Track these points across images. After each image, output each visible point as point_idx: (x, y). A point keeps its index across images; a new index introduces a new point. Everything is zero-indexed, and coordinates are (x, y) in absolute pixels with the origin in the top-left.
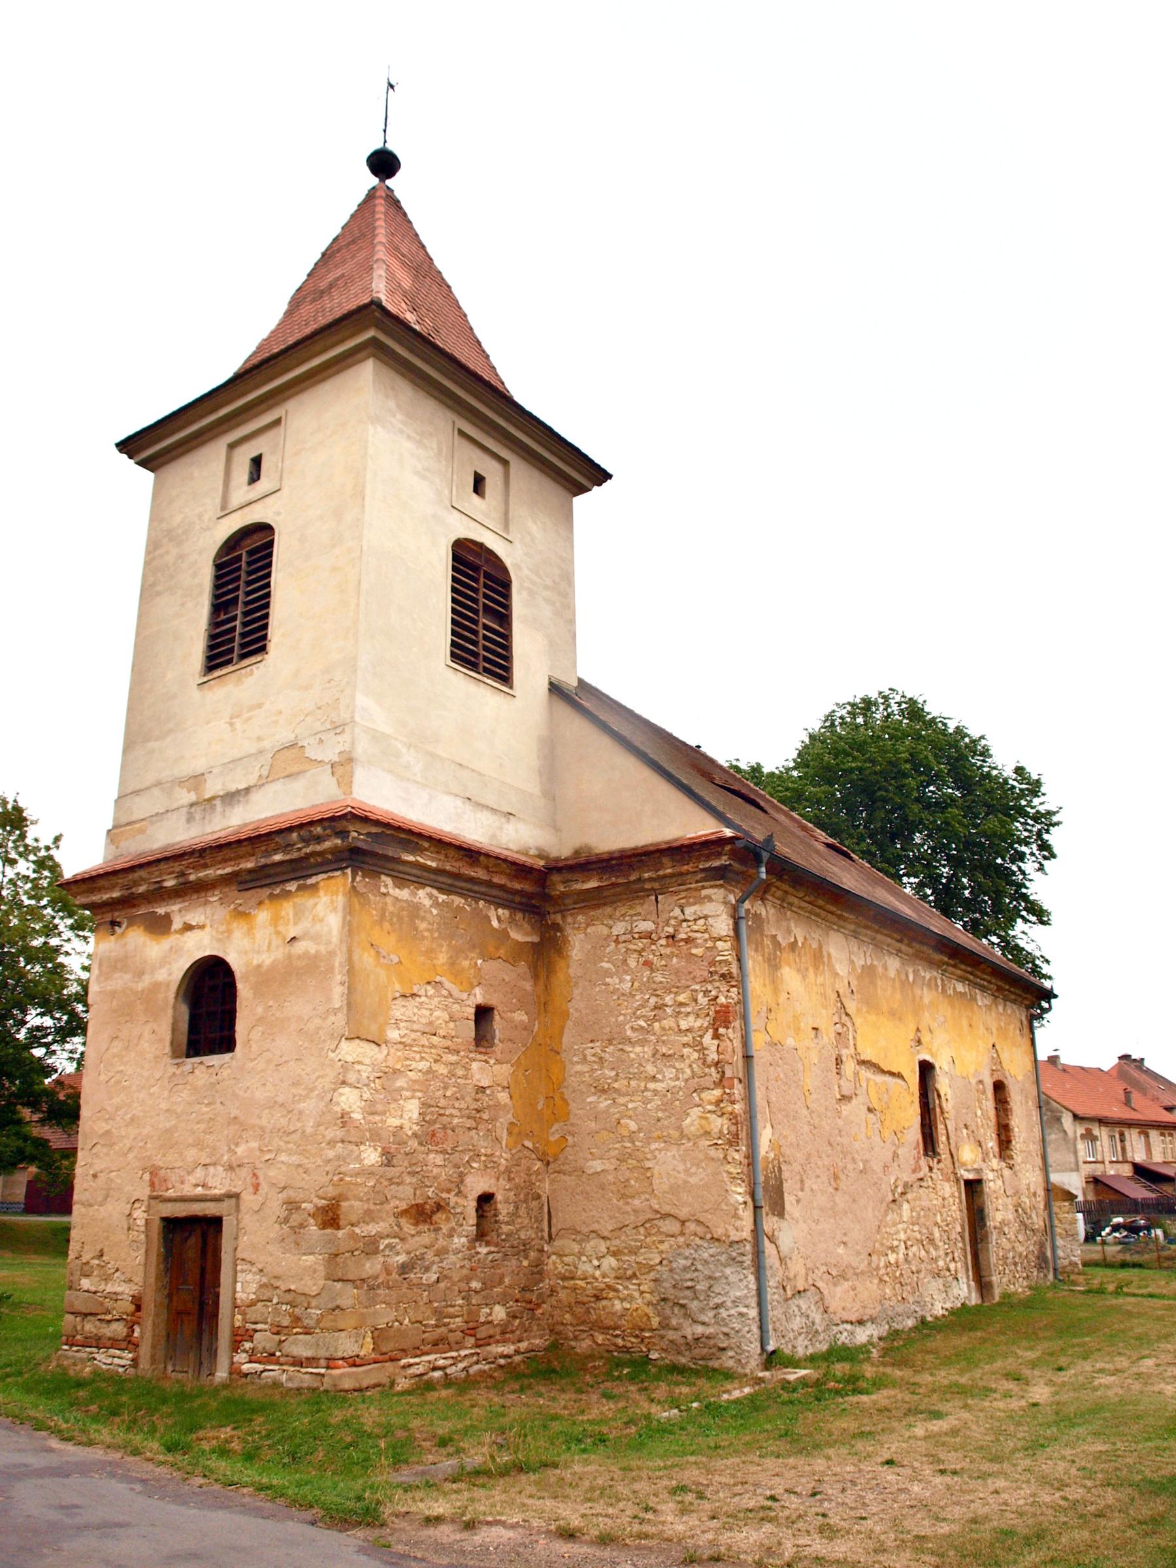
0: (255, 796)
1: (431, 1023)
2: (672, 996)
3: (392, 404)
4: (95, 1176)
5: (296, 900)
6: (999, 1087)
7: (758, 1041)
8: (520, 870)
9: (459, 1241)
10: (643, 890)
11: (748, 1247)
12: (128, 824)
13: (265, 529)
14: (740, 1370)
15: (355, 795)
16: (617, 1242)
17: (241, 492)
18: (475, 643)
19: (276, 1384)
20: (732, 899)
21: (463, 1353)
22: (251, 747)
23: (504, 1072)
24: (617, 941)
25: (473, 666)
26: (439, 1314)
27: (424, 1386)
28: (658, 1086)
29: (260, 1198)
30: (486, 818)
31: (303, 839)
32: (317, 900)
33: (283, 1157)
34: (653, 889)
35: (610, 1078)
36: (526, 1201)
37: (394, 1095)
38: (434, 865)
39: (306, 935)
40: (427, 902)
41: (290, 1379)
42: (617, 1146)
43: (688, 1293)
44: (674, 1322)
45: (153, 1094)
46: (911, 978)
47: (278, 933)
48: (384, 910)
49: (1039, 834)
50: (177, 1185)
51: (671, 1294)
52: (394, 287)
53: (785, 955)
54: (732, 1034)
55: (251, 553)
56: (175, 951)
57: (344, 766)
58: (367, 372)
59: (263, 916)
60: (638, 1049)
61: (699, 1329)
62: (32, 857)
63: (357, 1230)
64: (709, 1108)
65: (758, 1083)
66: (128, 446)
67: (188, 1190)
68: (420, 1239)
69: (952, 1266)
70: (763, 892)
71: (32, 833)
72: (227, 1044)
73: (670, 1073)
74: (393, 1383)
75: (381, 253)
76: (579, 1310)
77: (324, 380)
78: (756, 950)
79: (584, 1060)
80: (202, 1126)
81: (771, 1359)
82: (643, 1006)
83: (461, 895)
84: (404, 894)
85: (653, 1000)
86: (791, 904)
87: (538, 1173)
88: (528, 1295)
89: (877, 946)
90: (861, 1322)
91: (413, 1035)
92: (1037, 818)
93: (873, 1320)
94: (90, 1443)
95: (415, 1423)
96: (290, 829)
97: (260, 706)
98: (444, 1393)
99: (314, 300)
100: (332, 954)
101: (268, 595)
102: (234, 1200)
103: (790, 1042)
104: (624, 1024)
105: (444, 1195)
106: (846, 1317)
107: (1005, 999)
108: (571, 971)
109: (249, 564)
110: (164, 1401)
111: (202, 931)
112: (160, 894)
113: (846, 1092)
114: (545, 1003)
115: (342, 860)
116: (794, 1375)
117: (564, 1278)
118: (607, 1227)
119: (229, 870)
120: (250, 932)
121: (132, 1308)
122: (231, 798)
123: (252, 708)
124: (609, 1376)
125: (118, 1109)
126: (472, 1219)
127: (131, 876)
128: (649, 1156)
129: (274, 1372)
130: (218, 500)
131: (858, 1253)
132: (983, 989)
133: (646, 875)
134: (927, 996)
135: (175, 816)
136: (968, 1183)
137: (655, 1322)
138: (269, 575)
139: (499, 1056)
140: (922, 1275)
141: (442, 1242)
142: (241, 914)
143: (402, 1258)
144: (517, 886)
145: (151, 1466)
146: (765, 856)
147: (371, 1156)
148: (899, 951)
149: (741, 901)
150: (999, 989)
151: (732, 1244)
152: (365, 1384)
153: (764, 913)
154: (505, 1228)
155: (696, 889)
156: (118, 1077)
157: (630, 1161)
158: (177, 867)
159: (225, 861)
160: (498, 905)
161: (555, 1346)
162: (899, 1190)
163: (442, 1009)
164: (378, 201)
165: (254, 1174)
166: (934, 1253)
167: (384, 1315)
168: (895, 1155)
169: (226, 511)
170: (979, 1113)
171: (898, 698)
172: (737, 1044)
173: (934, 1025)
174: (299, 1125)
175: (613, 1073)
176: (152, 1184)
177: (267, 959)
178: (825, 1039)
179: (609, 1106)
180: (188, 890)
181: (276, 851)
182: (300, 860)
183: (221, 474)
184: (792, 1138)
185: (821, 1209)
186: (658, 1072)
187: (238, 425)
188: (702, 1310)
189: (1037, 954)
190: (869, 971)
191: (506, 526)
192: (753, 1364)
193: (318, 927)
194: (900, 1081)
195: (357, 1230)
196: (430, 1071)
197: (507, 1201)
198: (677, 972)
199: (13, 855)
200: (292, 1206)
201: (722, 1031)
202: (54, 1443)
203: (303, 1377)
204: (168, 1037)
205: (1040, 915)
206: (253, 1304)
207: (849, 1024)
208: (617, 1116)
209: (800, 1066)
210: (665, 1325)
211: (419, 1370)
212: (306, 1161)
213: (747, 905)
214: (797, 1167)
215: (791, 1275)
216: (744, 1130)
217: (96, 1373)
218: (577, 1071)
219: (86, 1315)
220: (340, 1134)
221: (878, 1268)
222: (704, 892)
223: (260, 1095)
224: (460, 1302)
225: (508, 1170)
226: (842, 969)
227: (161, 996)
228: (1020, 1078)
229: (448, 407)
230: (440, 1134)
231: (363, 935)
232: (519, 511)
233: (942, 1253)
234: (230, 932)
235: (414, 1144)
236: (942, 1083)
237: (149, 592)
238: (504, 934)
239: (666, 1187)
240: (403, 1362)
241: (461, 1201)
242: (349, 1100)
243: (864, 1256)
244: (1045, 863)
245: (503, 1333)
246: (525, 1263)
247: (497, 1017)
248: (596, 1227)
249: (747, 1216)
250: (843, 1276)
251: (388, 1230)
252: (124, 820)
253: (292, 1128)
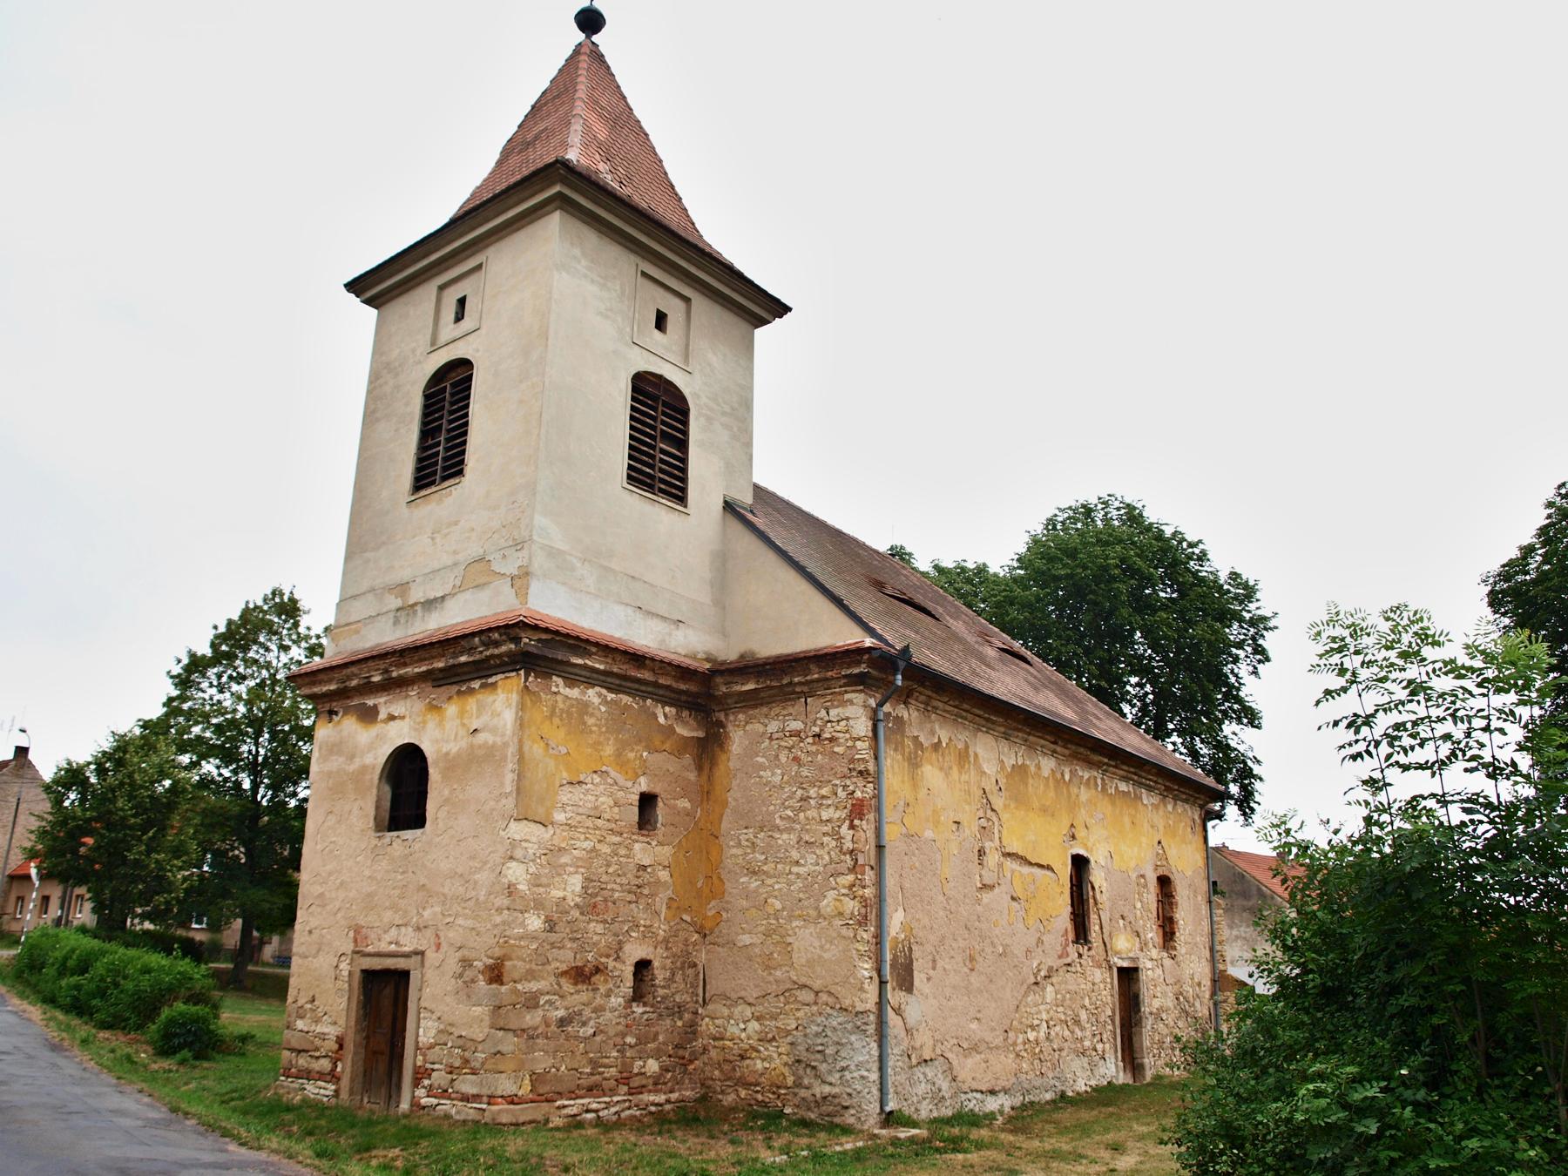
1: (596, 808)
3: (577, 252)
5: (480, 696)
6: (1164, 882)
7: (891, 833)
8: (683, 672)
9: (616, 1001)
10: (794, 693)
11: (872, 1018)
13: (464, 365)
14: (859, 1126)
15: (530, 605)
16: (760, 1008)
17: (448, 330)
18: (652, 467)
19: (447, 1116)
20: (872, 703)
21: (615, 1099)
22: (447, 560)
23: (666, 852)
24: (771, 738)
25: (650, 488)
26: (594, 1064)
27: (575, 1123)
29: (440, 956)
30: (657, 626)
31: (483, 643)
33: (460, 921)
36: (682, 968)
37: (558, 870)
38: (602, 667)
40: (596, 700)
41: (458, 1112)
43: (818, 1056)
44: (806, 1082)
46: (1067, 777)
47: (463, 725)
48: (554, 707)
49: (1254, 639)
51: (804, 1056)
52: (590, 140)
53: (927, 754)
54: (867, 826)
55: (453, 385)
56: (380, 738)
57: (521, 579)
58: (555, 221)
59: (452, 709)
60: (785, 836)
61: (827, 1089)
62: (304, 644)
63: (519, 987)
64: (844, 891)
65: (890, 869)
66: (356, 286)
67: (384, 947)
68: (578, 997)
69: (1099, 1047)
70: (905, 696)
71: (304, 621)
72: (418, 821)
73: (811, 859)
74: (547, 1121)
75: (580, 107)
76: (726, 1067)
77: (518, 229)
78: (896, 750)
79: (739, 845)
80: (397, 892)
81: (889, 1119)
82: (790, 798)
83: (628, 694)
84: (574, 693)
85: (800, 792)
86: (935, 708)
87: (695, 944)
88: (681, 1052)
89: (1031, 747)
90: (992, 1092)
91: (578, 818)
92: (1253, 622)
93: (1006, 1091)
94: (260, 1148)
95: (549, 1153)
96: (473, 634)
97: (456, 523)
98: (590, 1132)
99: (520, 152)
100: (506, 745)
101: (466, 424)
103: (929, 834)
105: (603, 960)
106: (975, 1086)
107: (1175, 799)
108: (731, 764)
109: (452, 395)
110: (353, 1126)
111: (404, 721)
112: (369, 688)
113: (987, 881)
114: (706, 793)
115: (516, 663)
116: (904, 1133)
117: (715, 1039)
118: (752, 994)
119: (424, 668)
120: (441, 724)
121: (336, 1047)
122: (430, 604)
123: (449, 525)
124: (744, 1127)
125: (330, 874)
126: (629, 981)
129: (446, 1106)
130: (429, 337)
131: (993, 1029)
132: (1149, 789)
134: (1085, 794)
135: (384, 619)
136: (1121, 970)
137: (790, 1080)
138: (467, 406)
139: (661, 838)
140: (1064, 1054)
141: (599, 1001)
142: (434, 708)
143: (561, 1013)
144: (683, 687)
145: (299, 1167)
146: (902, 664)
147: (535, 923)
148: (1054, 752)
149: (880, 705)
150: (1168, 789)
151: (857, 1014)
152: (521, 1120)
153: (906, 716)
154: (661, 992)
158: (382, 665)
159: (421, 660)
160: (665, 704)
161: (704, 1099)
162: (1043, 973)
163: (612, 796)
164: (583, 58)
166: (1079, 1034)
167: (542, 1062)
168: (1040, 941)
169: (435, 346)
170: (1139, 905)
171: (1117, 504)
172: (871, 834)
173: (1091, 822)
176: (356, 941)
177: (453, 748)
178: (967, 832)
180: (392, 685)
181: (462, 653)
182: (482, 661)
183: (432, 313)
184: (926, 921)
185: (954, 987)
187: (447, 269)
188: (830, 1072)
189: (1250, 755)
190: (1020, 770)
191: (686, 357)
192: (871, 1121)
193: (495, 721)
194: (1049, 873)
195: (519, 987)
196: (593, 850)
197: (664, 968)
198: (821, 768)
199: (287, 642)
200: (466, 963)
201: (856, 822)
202: (233, 1147)
203: (468, 1111)
204: (372, 813)
205: (1250, 717)
206: (431, 1047)
207: (995, 819)
209: (938, 856)
210: (798, 1084)
211: (574, 1111)
213: (887, 708)
214: (929, 948)
215: (918, 1045)
216: (874, 912)
217: (305, 1100)
218: (733, 854)
219: (300, 1051)
220: (506, 902)
221: (1015, 1044)
222: (847, 696)
223: (445, 866)
224: (615, 1054)
225: (666, 941)
226: (990, 768)
227: (368, 777)
228: (1189, 873)
229: (631, 250)
230: (601, 906)
231: (533, 728)
232: (700, 344)
233: (1088, 1033)
234: (424, 722)
235: (576, 913)
236: (1097, 876)
237: (370, 417)
238: (671, 729)
239: (803, 961)
240: (558, 1103)
241: (618, 965)
242: (516, 873)
243: (1000, 1032)
244: (1260, 667)
245: (655, 1084)
246: (680, 1023)
247: (660, 804)
248: (743, 994)
249: (872, 991)
250: (975, 1049)
251: (549, 988)
252: (343, 622)
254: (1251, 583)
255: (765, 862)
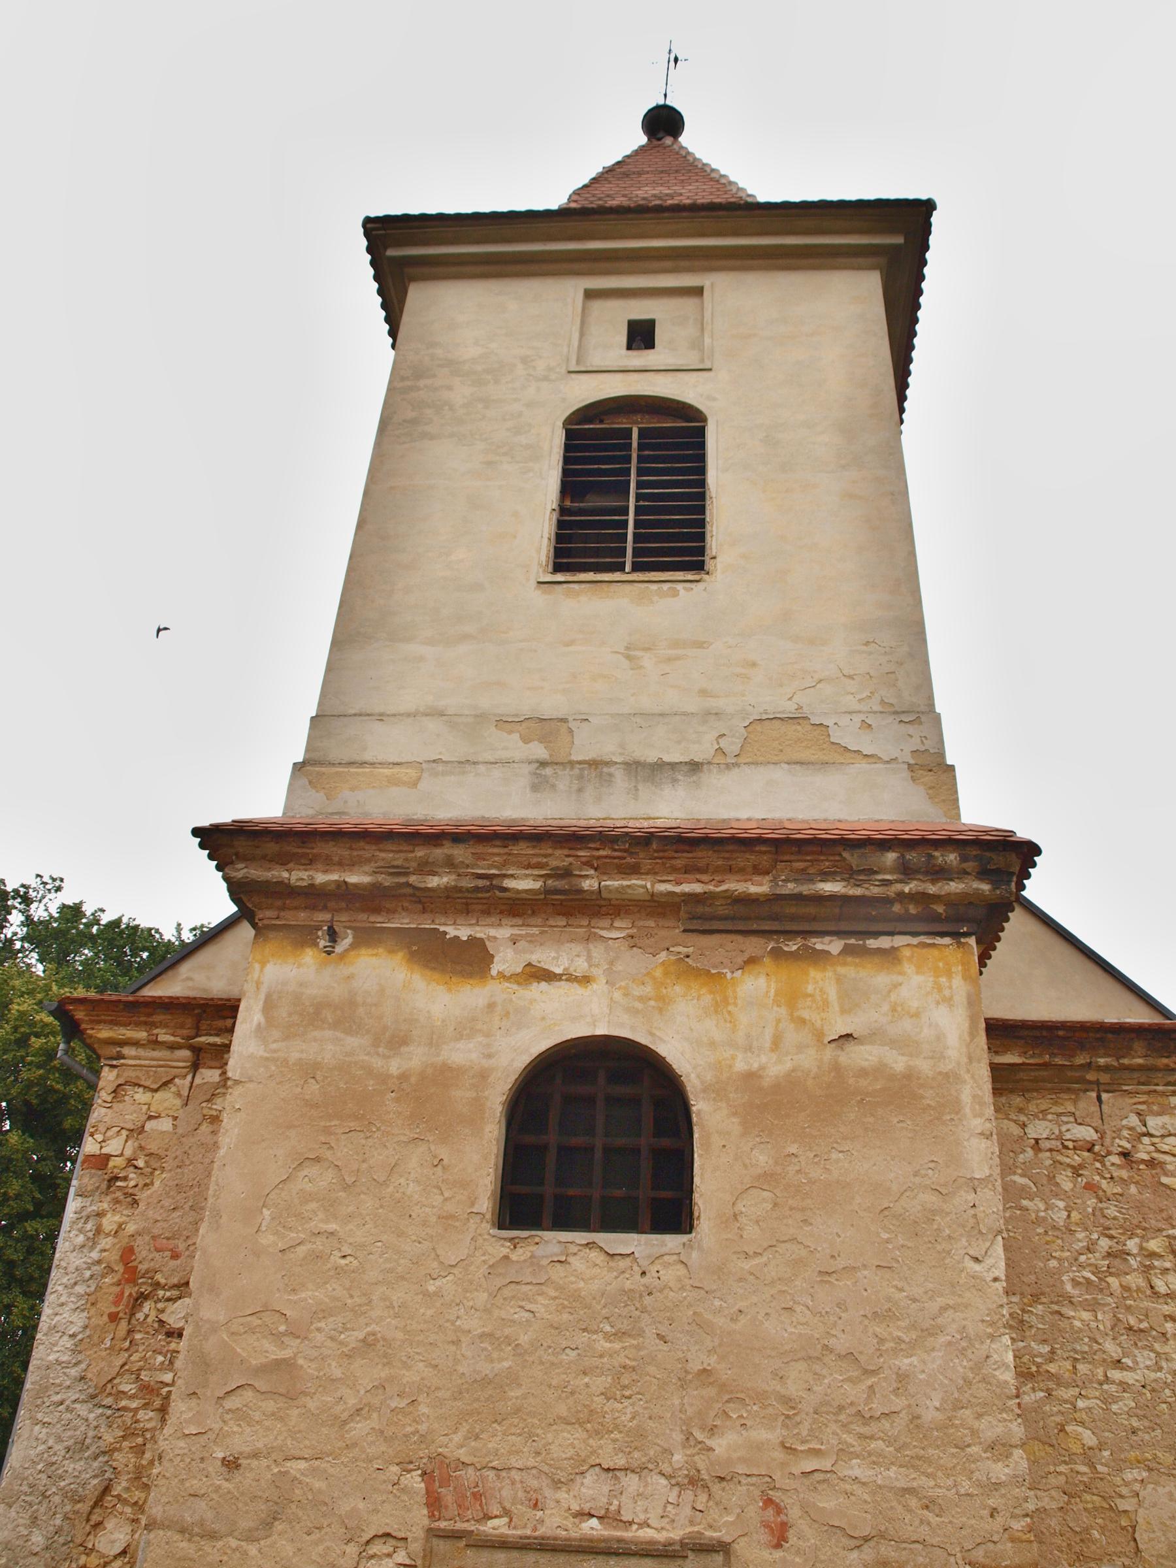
0: (714, 779)
2: (1137, 1240)
4: (231, 1464)
12: (351, 764)
28: (1129, 1377)
32: (896, 978)
34: (1098, 1083)
35: (1041, 1355)
39: (875, 1036)
42: (1062, 1468)
45: (438, 1294)
50: (519, 1509)
73: (1145, 1358)
96: (884, 844)
102: (719, 1558)
104: (1059, 1272)
115: (961, 920)
127: (420, 853)
128: (1124, 1491)
133: (1102, 1061)
155: (1163, 1094)
156: (319, 1244)
157: (1088, 1497)
158: (559, 858)
165: (769, 1502)
174: (898, 1403)
175: (1045, 1349)
176: (434, 1503)
179: (1040, 1403)
180: (565, 906)
181: (826, 876)
186: (1125, 1355)
198: (1139, 1206)
208: (1059, 1419)
212: (923, 1481)
239: (1162, 1548)
253: (878, 1407)
254: (404, 1049)
255: (1051, 1357)
